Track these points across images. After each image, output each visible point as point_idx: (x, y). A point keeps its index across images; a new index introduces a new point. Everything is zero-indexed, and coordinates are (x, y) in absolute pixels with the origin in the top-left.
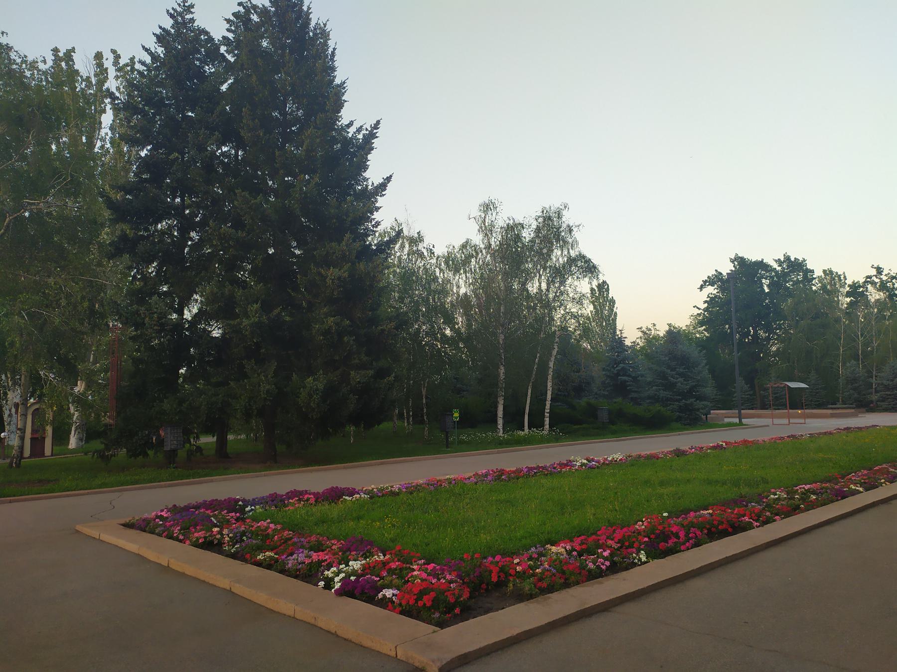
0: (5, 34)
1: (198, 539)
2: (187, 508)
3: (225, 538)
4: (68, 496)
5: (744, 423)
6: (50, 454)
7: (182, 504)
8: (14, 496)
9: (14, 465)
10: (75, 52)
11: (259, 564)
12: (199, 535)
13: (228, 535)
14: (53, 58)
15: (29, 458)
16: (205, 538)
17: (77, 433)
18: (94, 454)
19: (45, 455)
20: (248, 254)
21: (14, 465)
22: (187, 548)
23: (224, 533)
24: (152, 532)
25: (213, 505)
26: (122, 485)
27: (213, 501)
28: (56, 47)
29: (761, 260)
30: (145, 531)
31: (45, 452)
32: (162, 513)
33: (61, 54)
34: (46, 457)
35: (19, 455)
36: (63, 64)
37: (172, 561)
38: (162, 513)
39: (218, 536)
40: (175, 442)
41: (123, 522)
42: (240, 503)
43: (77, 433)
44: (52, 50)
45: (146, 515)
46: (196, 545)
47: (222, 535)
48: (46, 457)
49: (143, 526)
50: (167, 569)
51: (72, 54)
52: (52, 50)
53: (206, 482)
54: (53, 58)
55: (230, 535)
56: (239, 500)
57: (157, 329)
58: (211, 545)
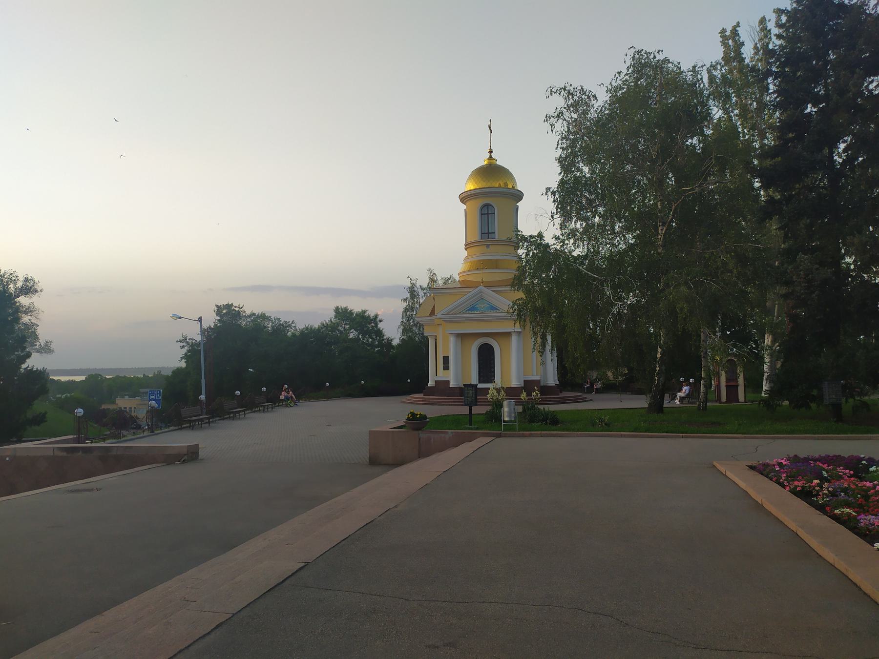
0: (660, 52)
1: (796, 487)
2: (806, 460)
3: (823, 491)
4: (728, 438)
5: (740, 401)
6: (743, 401)
7: (802, 455)
8: (686, 433)
9: (702, 408)
10: (739, 26)
11: (837, 519)
12: (799, 484)
13: (828, 489)
14: (721, 40)
15: (725, 402)
16: (803, 487)
17: (768, 383)
18: (759, 403)
19: (740, 401)
20: (543, 272)
21: (702, 408)
22: (785, 494)
23: (824, 486)
24: (767, 476)
25: (833, 460)
26: (777, 433)
27: (835, 456)
28: (723, 29)
29: (372, 315)
30: (762, 474)
31: (739, 398)
32: (782, 461)
33: (728, 33)
34: (740, 402)
35: (705, 400)
36: (730, 42)
37: (764, 500)
38: (782, 461)
39: (817, 488)
40: (833, 396)
41: (750, 464)
42: (864, 462)
43: (768, 383)
44: (217, 306)
45: (768, 461)
46: (794, 492)
47: (822, 488)
48: (740, 402)
49: (763, 470)
50: (759, 507)
51: (738, 29)
52: (217, 306)
53: (859, 439)
54: (721, 40)
55: (830, 489)
56: (863, 459)
57: (805, 286)
58: (806, 495)
